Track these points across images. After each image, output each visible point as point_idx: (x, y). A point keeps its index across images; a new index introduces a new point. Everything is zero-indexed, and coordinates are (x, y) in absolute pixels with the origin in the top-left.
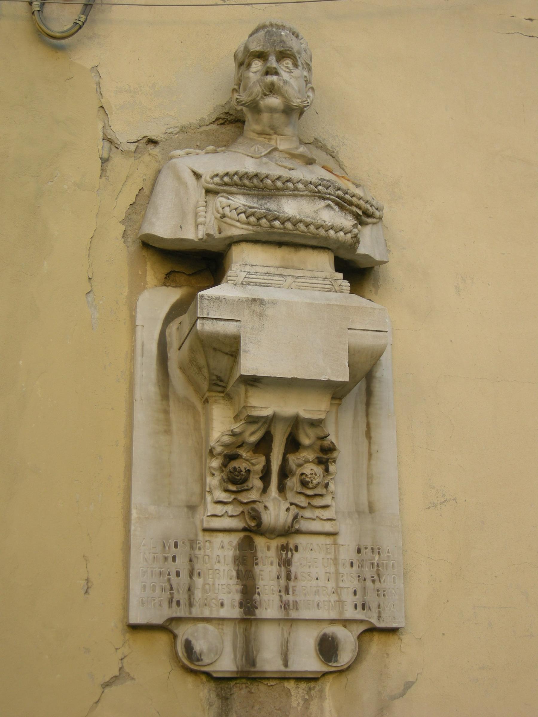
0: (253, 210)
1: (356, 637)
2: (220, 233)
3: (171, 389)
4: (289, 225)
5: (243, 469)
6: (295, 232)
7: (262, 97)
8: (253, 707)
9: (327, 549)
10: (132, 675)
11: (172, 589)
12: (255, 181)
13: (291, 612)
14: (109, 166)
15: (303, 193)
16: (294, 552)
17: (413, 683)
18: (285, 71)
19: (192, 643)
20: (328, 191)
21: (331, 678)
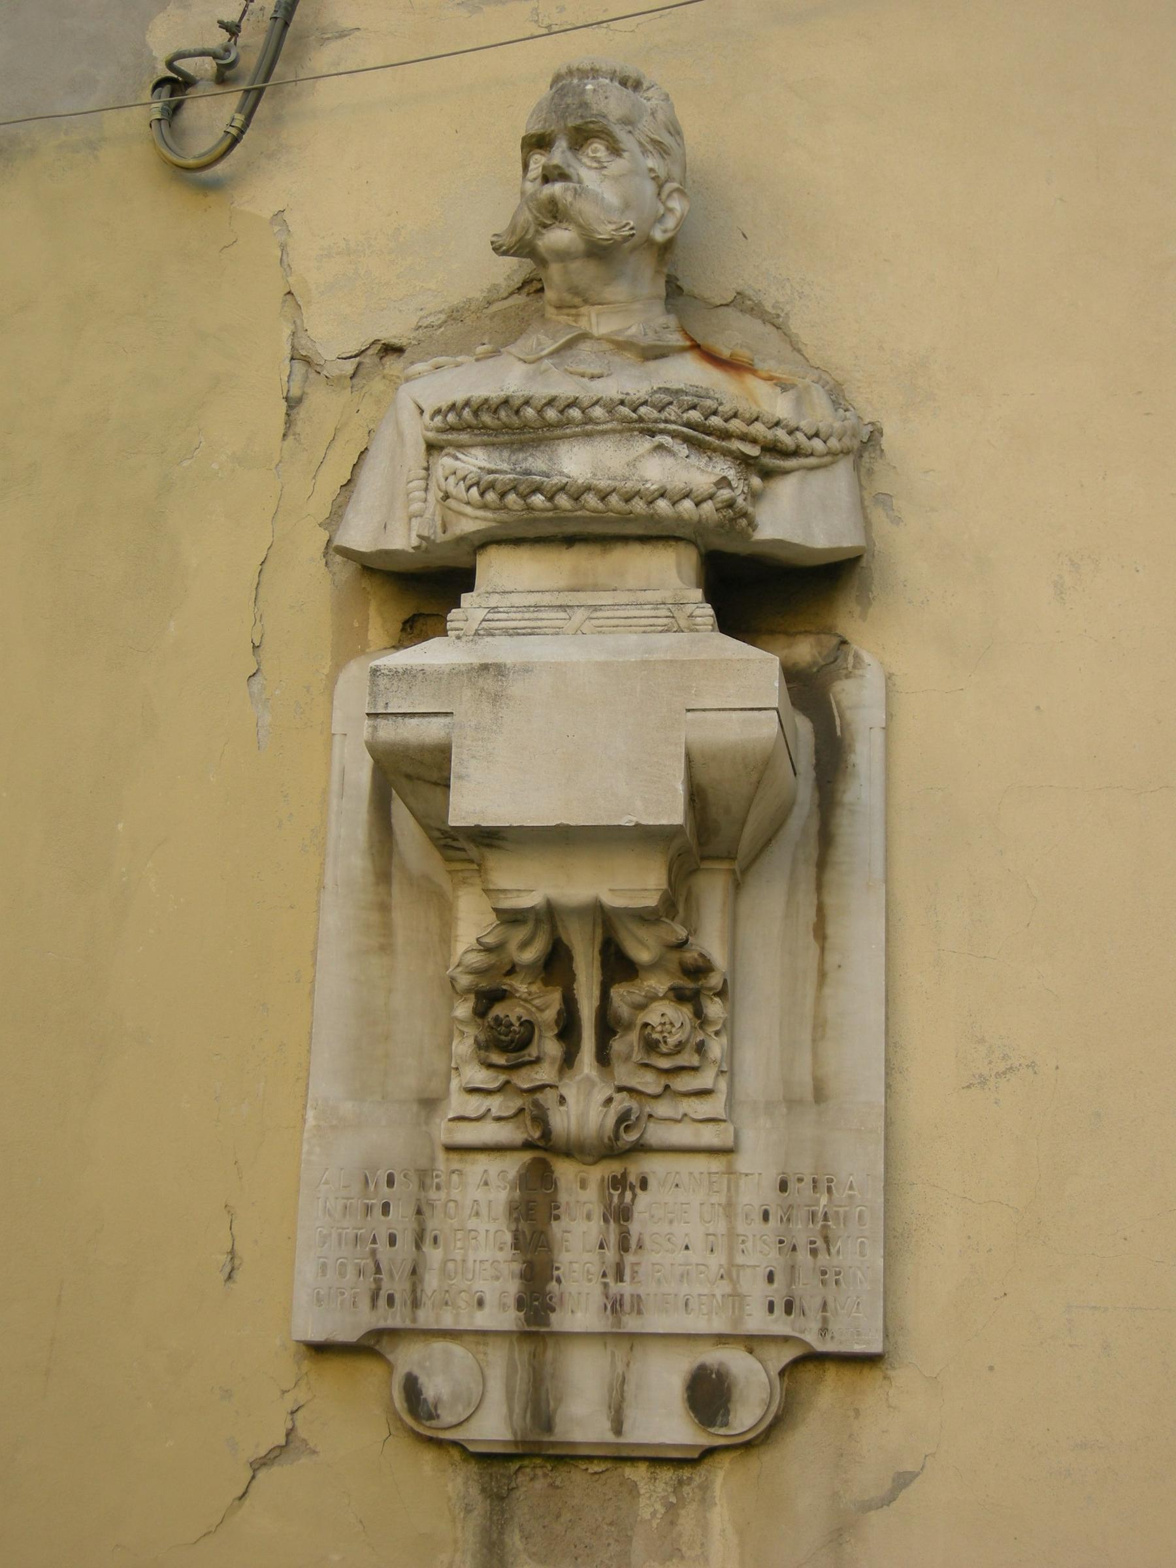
0: (491, 477)
1: (774, 1373)
2: (444, 532)
3: (395, 860)
4: (563, 501)
5: (513, 1019)
6: (579, 513)
7: (537, 232)
8: (558, 1516)
9: (711, 1183)
10: (311, 1445)
11: (378, 1270)
12: (503, 414)
13: (625, 1319)
14: (301, 413)
15: (604, 427)
16: (638, 1191)
17: (913, 1476)
18: (590, 168)
19: (420, 1381)
20: (663, 416)
21: (725, 1462)
